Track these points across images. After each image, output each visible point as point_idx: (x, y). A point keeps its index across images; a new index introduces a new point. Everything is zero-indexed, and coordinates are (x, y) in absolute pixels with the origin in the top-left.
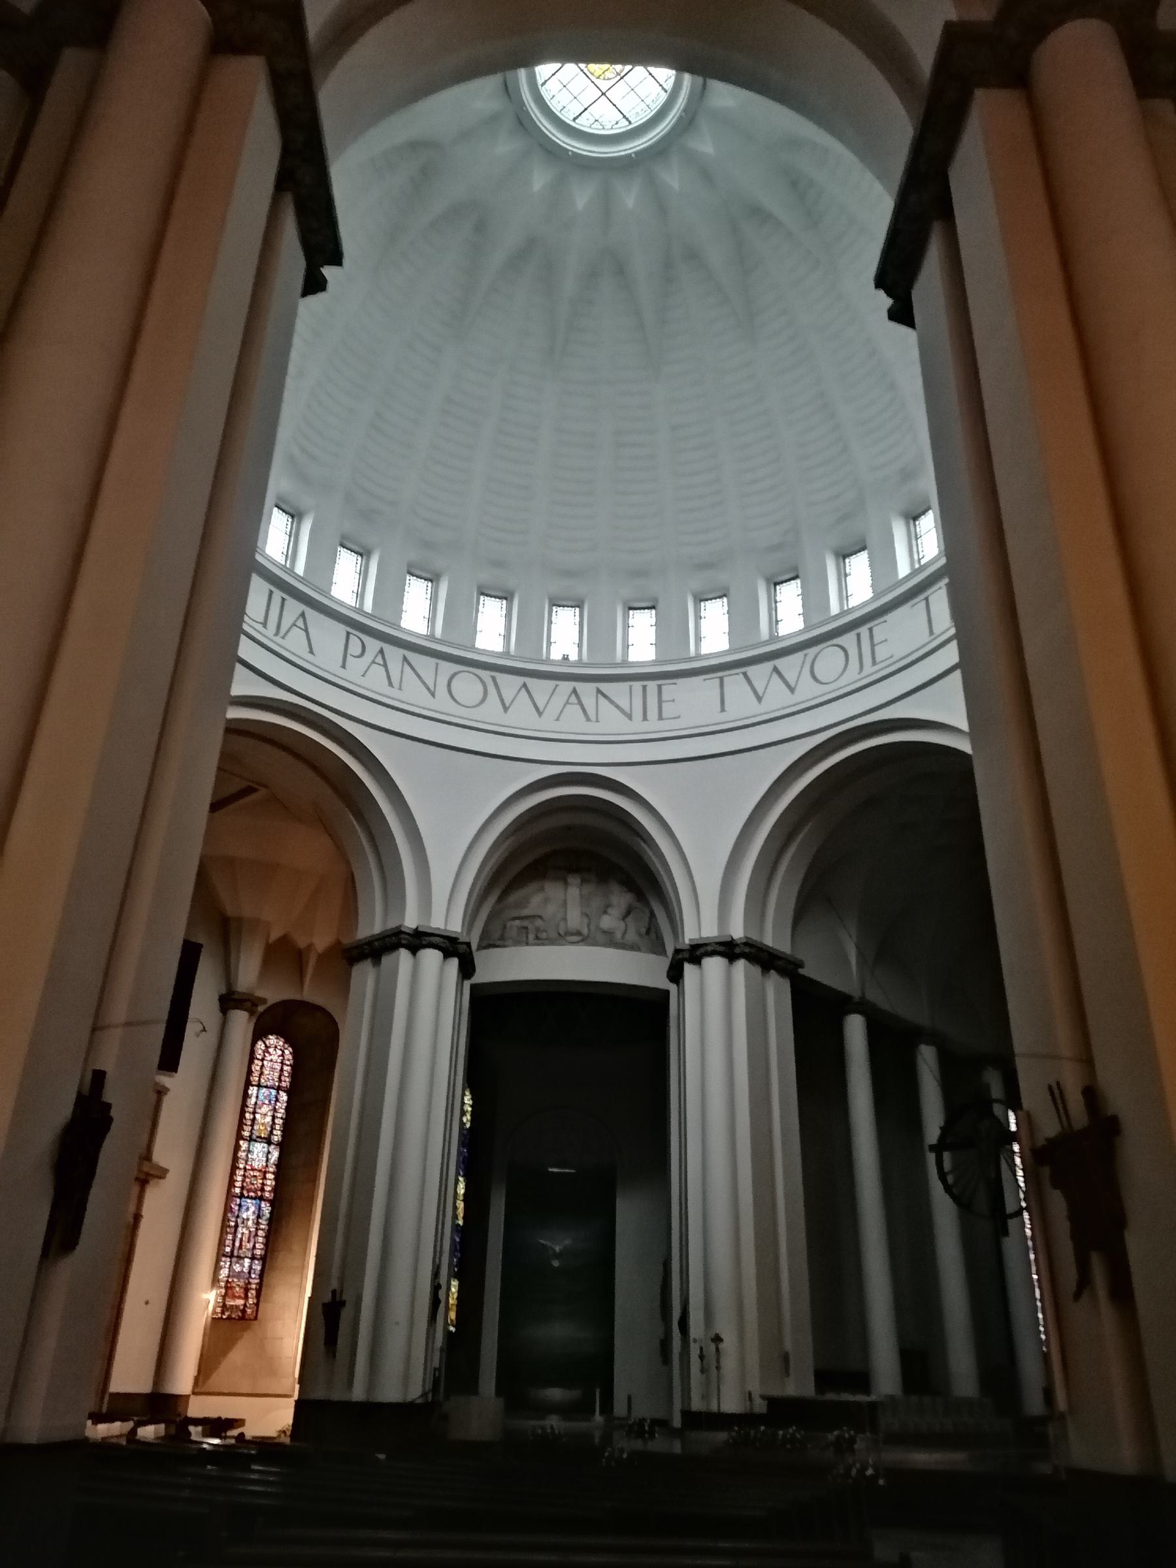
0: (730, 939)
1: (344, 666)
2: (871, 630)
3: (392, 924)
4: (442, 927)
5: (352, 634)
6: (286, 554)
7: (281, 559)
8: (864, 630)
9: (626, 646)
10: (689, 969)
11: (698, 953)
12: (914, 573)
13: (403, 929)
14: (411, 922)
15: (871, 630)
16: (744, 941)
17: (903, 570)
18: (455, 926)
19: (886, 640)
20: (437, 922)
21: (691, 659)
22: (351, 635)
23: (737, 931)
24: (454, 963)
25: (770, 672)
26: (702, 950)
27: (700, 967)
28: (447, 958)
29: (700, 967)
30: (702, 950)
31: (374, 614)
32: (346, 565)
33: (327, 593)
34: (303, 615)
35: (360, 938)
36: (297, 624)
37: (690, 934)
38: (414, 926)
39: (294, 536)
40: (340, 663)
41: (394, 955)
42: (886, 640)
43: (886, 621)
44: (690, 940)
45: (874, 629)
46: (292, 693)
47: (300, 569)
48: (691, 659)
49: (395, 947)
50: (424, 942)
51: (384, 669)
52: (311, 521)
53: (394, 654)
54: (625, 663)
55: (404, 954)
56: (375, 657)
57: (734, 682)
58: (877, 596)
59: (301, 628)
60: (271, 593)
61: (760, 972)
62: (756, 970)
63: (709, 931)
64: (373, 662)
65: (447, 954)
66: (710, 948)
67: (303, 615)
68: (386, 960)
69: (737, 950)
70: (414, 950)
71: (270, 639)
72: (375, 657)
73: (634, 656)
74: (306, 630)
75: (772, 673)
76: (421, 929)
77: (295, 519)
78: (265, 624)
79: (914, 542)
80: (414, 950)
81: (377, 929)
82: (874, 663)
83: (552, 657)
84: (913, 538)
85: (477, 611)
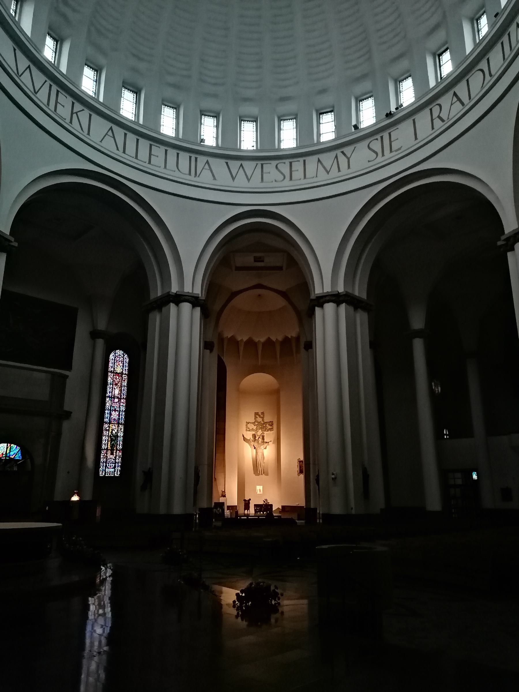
0: (337, 293)
1: (215, 179)
2: (390, 134)
3: (166, 291)
4: (191, 292)
6: (134, 114)
7: (91, 94)
8: (386, 135)
9: (280, 141)
10: (318, 310)
11: (322, 300)
12: (438, 84)
13: (170, 294)
14: (175, 289)
15: (390, 134)
16: (345, 293)
17: (432, 83)
18: (198, 291)
20: (188, 289)
21: (314, 145)
23: (341, 289)
24: (198, 310)
25: (516, 28)
26: (324, 299)
27: (323, 309)
28: (194, 307)
29: (323, 309)
30: (324, 299)
31: (104, 103)
32: (88, 74)
33: (118, 113)
34: (111, 129)
35: (152, 299)
37: (318, 291)
39: (98, 81)
40: (212, 178)
41: (167, 307)
43: (398, 128)
45: (391, 133)
46: (108, 171)
47: (141, 121)
48: (314, 145)
50: (182, 299)
52: (106, 70)
54: (279, 149)
55: (172, 306)
58: (418, 99)
59: (111, 137)
61: (353, 310)
62: (351, 309)
63: (328, 289)
65: (194, 306)
66: (327, 298)
68: (164, 309)
69: (341, 299)
70: (177, 304)
71: (98, 144)
73: (284, 145)
74: (114, 137)
75: (517, 29)
77: (98, 72)
79: (477, 34)
80: (177, 304)
82: (391, 151)
83: (242, 148)
84: (438, 66)
85: (201, 124)
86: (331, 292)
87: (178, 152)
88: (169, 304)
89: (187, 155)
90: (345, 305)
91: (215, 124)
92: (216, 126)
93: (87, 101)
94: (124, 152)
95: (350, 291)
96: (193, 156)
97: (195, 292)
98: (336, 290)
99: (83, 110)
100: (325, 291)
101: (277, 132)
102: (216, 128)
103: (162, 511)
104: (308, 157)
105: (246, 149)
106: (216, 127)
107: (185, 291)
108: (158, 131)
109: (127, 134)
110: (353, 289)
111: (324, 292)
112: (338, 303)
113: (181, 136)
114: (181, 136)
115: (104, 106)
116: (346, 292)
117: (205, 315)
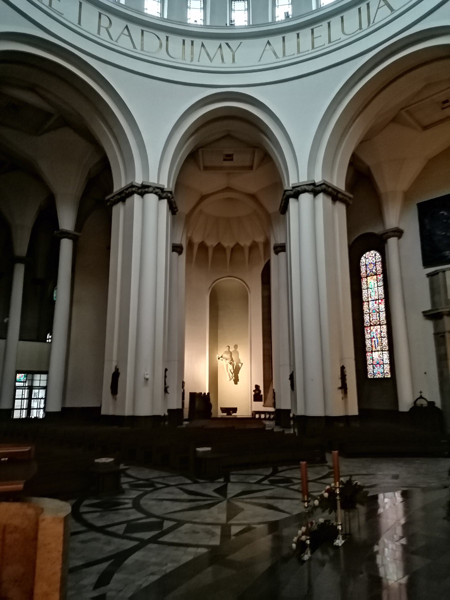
0: (314, 182)
4: (156, 182)
5: (103, 14)
10: (292, 202)
13: (134, 184)
14: (139, 180)
19: (320, 36)
20: (153, 180)
22: (102, 15)
23: (318, 179)
24: (165, 202)
36: (124, 33)
38: (140, 183)
42: (320, 36)
44: (292, 184)
49: (132, 193)
51: (129, 38)
53: (135, 30)
55: (136, 197)
56: (123, 31)
57: (291, 37)
60: (184, 41)
62: (329, 200)
63: (304, 179)
64: (122, 33)
65: (161, 198)
67: (127, 27)
68: (128, 201)
69: (319, 188)
70: (142, 195)
72: (123, 31)
76: (144, 184)
78: (184, 59)
80: (142, 195)
81: (123, 185)
86: (307, 181)
87: (184, 38)
88: (133, 196)
89: (180, 39)
90: (323, 197)
91: (246, 7)
92: (247, 9)
93: (318, 16)
94: (142, 49)
95: (328, 180)
96: (188, 41)
97: (160, 183)
98: (312, 179)
99: (241, 43)
100: (301, 180)
101: (314, 14)
102: (247, 11)
103: (128, 412)
104: (287, 34)
105: (188, 18)
106: (247, 10)
107: (150, 181)
108: (141, 12)
109: (276, 59)
110: (332, 177)
111: (300, 182)
112: (315, 193)
113: (166, 16)
114: (166, 16)
115: (299, 18)
116: (324, 181)
117: (173, 208)
